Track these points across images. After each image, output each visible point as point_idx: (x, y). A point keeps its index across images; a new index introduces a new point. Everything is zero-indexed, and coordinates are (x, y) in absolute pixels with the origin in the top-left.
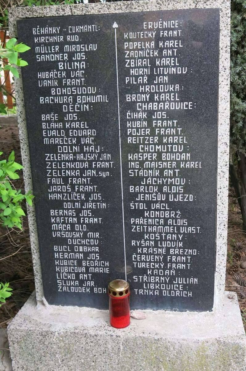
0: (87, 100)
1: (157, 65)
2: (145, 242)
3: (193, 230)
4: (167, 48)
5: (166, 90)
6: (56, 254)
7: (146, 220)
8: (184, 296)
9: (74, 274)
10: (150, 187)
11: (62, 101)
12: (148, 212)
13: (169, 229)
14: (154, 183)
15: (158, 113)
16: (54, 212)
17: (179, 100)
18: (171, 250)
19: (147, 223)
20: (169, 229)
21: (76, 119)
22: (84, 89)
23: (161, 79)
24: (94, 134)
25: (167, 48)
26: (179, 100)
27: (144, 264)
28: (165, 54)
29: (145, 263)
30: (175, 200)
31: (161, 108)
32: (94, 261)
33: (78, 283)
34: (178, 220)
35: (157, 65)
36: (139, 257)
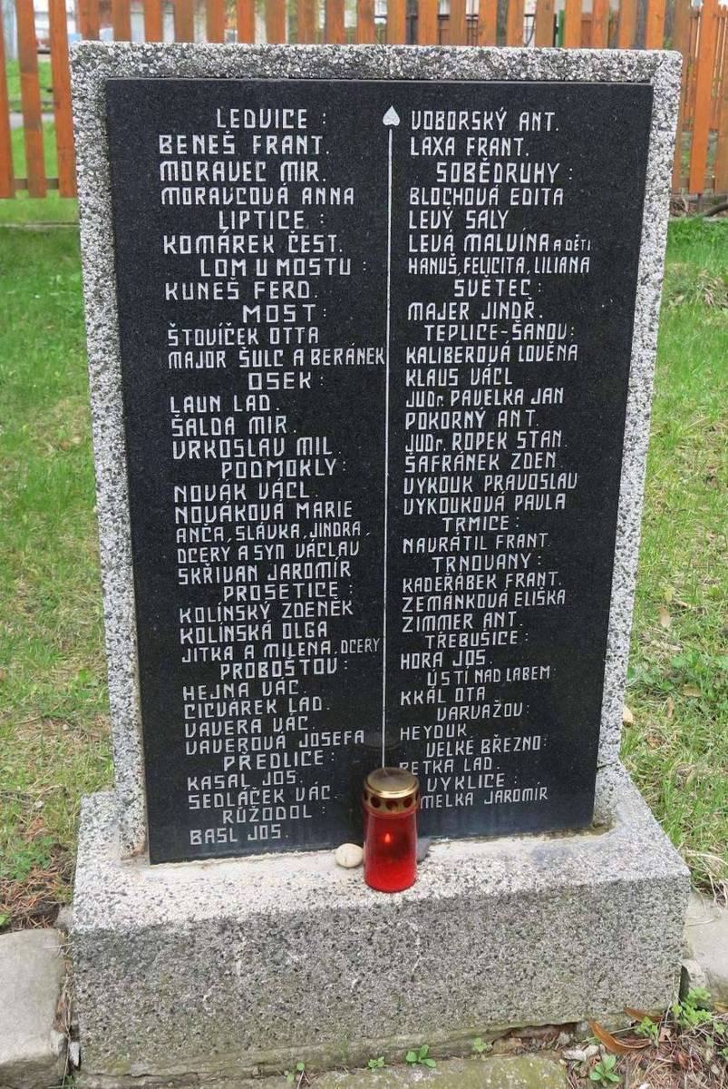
1: (268, 152)
2: (522, 329)
3: (244, 633)
5: (278, 452)
6: (283, 200)
7: (481, 579)
8: (280, 227)
9: (272, 342)
10: (217, 261)
11: (256, 515)
12: (174, 238)
13: (263, 425)
14: (288, 124)
15: (425, 428)
17: (235, 840)
18: (225, 812)
19: (189, 149)
20: (263, 425)
21: (256, 547)
22: (256, 466)
23: (501, 560)
24: (265, 406)
26: (235, 840)
27: (239, 241)
28: (524, 125)
29: (242, 237)
30: (292, 112)
31: (285, 575)
32: (254, 525)
33: (246, 691)
34: (272, 330)
35: (268, 152)
36: (306, 240)
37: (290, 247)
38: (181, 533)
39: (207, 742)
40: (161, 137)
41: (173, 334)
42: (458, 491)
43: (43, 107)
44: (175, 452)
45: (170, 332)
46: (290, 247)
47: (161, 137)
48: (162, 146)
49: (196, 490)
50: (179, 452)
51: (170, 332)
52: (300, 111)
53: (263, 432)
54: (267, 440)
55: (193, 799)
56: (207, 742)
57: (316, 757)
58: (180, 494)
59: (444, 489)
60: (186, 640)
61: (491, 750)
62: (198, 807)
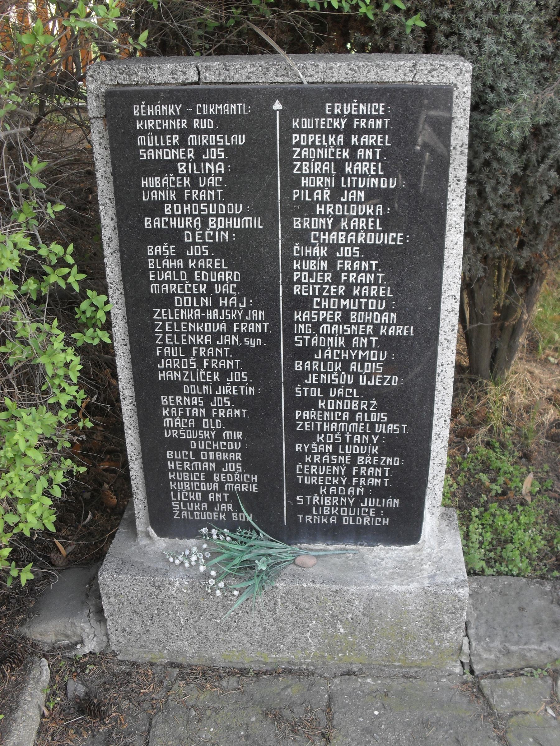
0: (320, 225)
4: (365, 147)
16: (168, 400)
25: (365, 147)
37: (312, 238)
38: (353, 365)
39: (361, 414)
40: (296, 362)
41: (298, 390)
42: (215, 213)
43: (178, 120)
44: (377, 429)
45: (297, 388)
46: (312, 238)
47: (296, 362)
48: (296, 367)
49: (230, 211)
50: (168, 434)
51: (297, 388)
52: (399, 235)
53: (382, 234)
54: (354, 234)
55: (298, 339)
56: (361, 414)
57: (399, 239)
58: (203, 302)
59: (315, 226)
60: (298, 319)
61: (161, 185)
62: (301, 345)
